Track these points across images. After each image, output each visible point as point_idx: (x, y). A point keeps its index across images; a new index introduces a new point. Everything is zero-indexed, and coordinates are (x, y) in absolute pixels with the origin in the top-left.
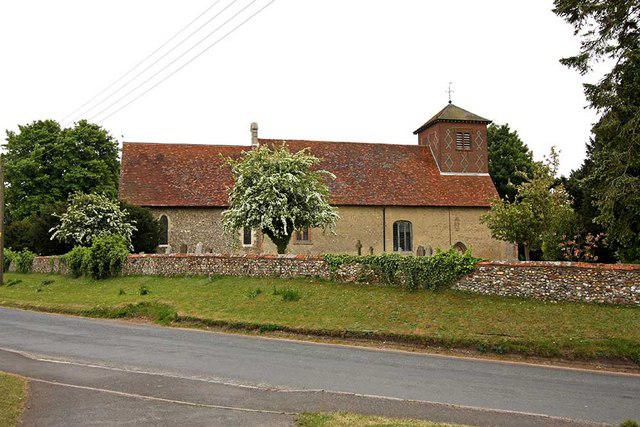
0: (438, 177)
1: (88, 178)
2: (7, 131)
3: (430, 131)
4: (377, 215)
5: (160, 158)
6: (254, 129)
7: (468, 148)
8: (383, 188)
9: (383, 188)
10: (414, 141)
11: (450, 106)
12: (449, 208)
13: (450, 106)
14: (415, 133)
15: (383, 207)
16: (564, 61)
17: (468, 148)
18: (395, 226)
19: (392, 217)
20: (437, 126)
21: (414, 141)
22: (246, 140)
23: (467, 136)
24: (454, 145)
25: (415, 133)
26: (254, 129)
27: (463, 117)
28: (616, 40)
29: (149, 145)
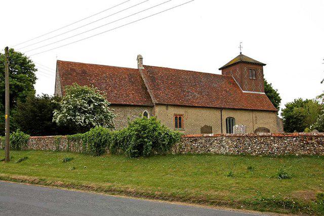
0: (242, 93)
1: (18, 86)
2: (7, 48)
3: (232, 69)
4: (218, 113)
5: (84, 72)
6: (140, 59)
7: (254, 78)
8: (218, 98)
9: (218, 98)
10: (220, 73)
11: (241, 55)
12: (253, 111)
13: (241, 55)
14: (220, 69)
15: (221, 109)
16: (265, 65)
17: (254, 78)
18: (226, 120)
19: (226, 115)
20: (240, 64)
21: (220, 73)
22: (134, 65)
23: (254, 72)
24: (248, 76)
25: (220, 69)
26: (140, 59)
27: (251, 61)
28: (51, 93)
29: (75, 64)
